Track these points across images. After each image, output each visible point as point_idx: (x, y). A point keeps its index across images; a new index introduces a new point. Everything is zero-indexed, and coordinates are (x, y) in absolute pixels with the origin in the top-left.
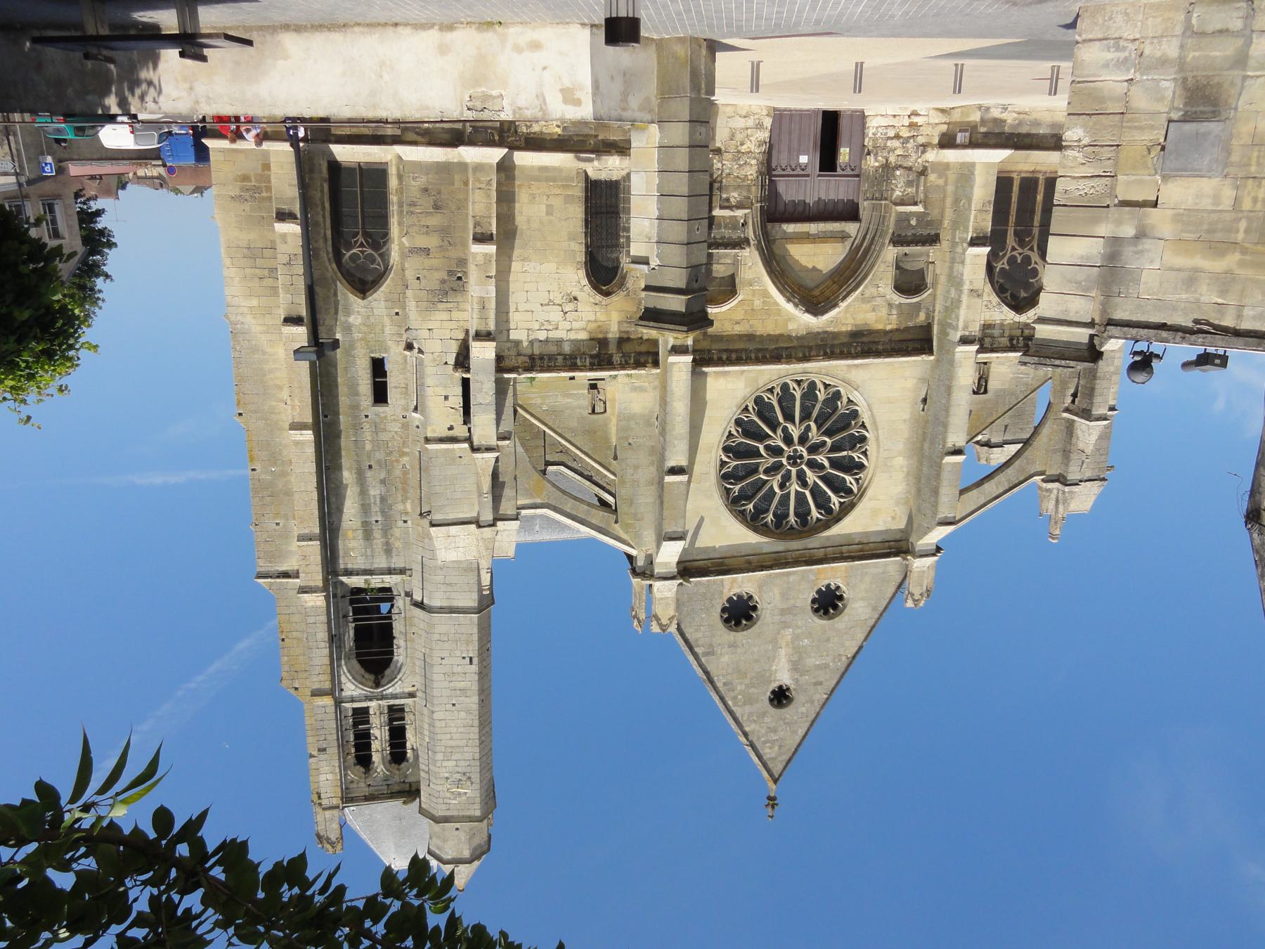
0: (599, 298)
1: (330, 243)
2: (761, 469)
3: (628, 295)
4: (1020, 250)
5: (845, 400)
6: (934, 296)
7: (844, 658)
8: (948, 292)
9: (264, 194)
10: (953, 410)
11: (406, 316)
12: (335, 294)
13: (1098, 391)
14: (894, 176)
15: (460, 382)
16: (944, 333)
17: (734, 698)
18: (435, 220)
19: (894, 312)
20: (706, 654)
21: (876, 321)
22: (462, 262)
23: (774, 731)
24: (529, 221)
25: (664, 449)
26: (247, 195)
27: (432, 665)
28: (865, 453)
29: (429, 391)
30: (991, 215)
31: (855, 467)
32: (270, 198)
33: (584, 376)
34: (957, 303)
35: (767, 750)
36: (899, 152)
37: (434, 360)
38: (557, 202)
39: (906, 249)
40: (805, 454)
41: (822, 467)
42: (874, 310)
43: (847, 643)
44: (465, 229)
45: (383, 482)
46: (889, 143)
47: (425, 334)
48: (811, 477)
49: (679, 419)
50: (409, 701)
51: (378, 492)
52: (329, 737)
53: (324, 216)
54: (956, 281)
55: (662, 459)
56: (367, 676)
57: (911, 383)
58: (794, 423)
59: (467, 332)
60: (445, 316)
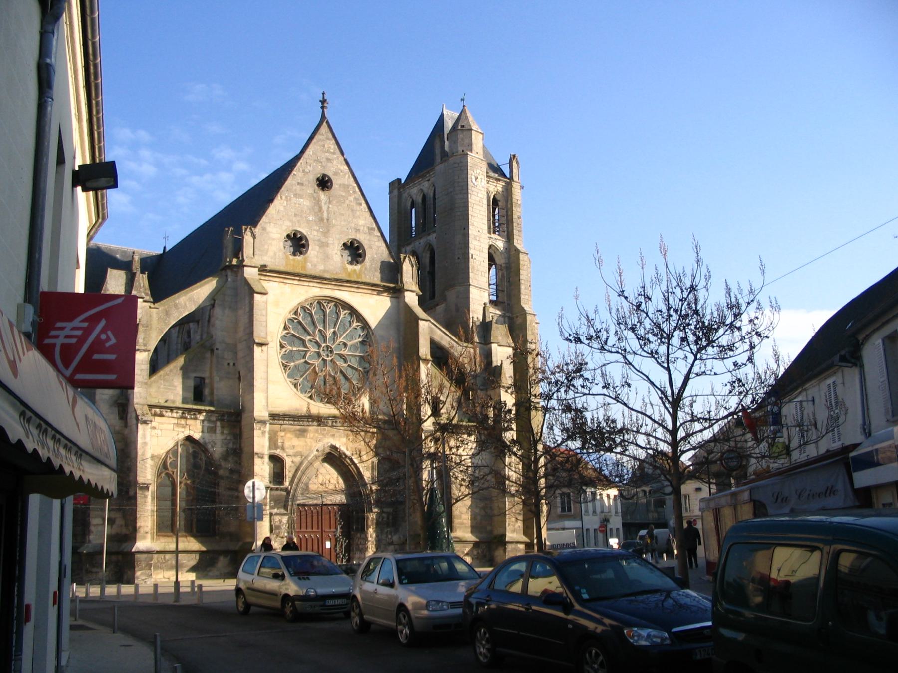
12: (390, 253)
17: (355, 192)
19: (280, 444)
35: (332, 146)
42: (294, 447)
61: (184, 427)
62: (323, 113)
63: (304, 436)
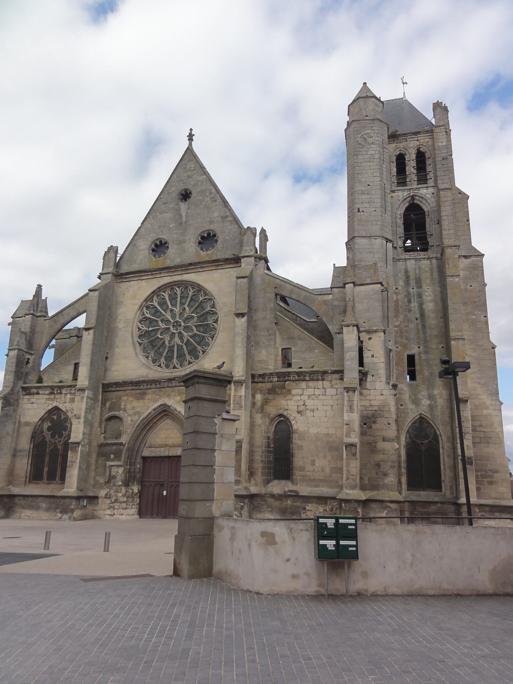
0: (285, 413)
1: (441, 446)
2: (196, 319)
3: (269, 415)
4: (56, 441)
5: (150, 358)
6: (101, 415)
7: (151, 217)
8: (93, 418)
9: (479, 473)
10: (90, 352)
11: (396, 404)
13: (14, 365)
14: (123, 482)
15: (365, 365)
16: (95, 395)
17: (211, 193)
18: (379, 457)
19: (123, 407)
20: (226, 217)
21: (132, 401)
22: (363, 433)
23: (189, 177)
24: (325, 456)
25: (248, 328)
26: (490, 473)
27: (381, 207)
28: (139, 329)
29: (383, 359)
30: (69, 459)
31: (144, 320)
32: (476, 472)
33: (294, 369)
34: (88, 410)
36: (120, 494)
37: (380, 377)
38: (309, 467)
39: (116, 441)
40: (172, 328)
41: (162, 321)
42: (134, 407)
43: (149, 226)
44: (362, 452)
45: (410, 311)
46: (125, 499)
47: (384, 392)
48: (168, 316)
49: (239, 345)
50: (394, 188)
51: (412, 305)
52: (440, 166)
53: (444, 460)
54: (88, 423)
55: (249, 322)
56: (419, 203)
57: (114, 368)
58: (178, 345)
59: (361, 394)
60: (374, 403)
61: (53, 400)
62: (190, 144)
63: (143, 399)
